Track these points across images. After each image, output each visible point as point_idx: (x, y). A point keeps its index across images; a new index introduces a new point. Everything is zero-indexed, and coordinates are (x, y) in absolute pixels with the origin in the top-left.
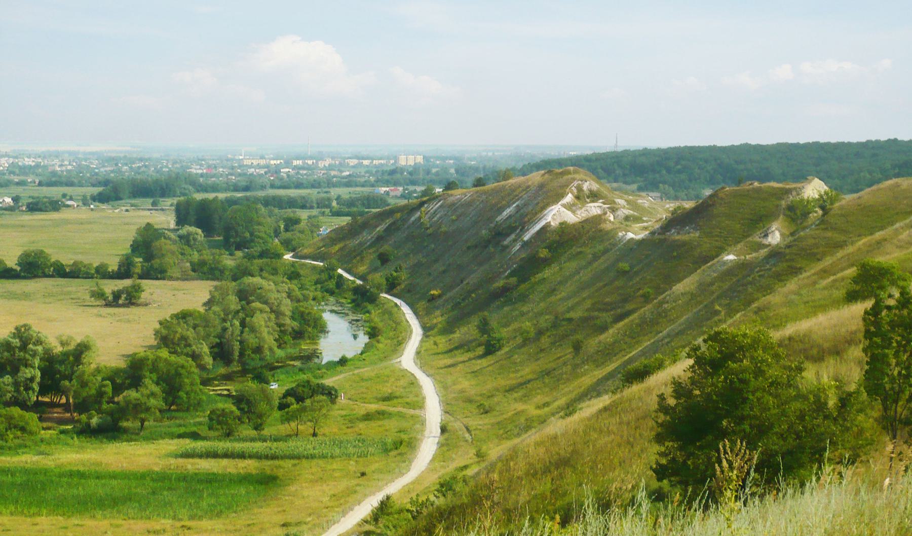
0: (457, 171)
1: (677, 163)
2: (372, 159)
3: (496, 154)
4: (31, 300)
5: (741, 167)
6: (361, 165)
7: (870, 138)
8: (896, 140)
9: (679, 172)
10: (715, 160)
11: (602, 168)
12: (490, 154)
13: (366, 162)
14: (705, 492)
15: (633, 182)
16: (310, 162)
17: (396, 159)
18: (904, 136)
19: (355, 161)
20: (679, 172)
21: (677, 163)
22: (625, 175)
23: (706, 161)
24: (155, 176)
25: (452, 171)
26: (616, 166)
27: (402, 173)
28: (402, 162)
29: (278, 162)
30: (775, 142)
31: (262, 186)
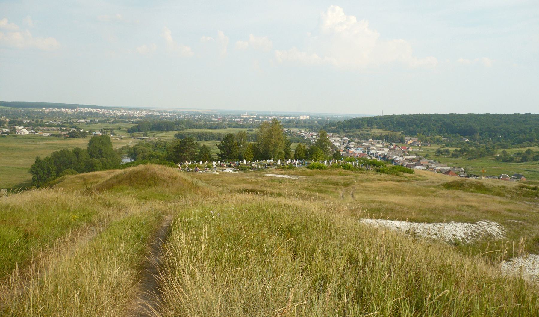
0: (318, 122)
1: (421, 122)
2: (290, 117)
3: (339, 116)
4: (245, 172)
5: (456, 125)
6: (285, 118)
7: (378, 115)
8: (529, 114)
9: (422, 126)
10: (441, 121)
11: (383, 123)
12: (336, 116)
13: (287, 118)
14: (156, 277)
15: (399, 131)
16: (266, 117)
17: (299, 117)
18: (535, 110)
19: (284, 117)
20: (422, 126)
21: (421, 122)
22: (394, 127)
23: (436, 121)
24: (340, 117)
25: (316, 122)
26: (389, 122)
27: (293, 122)
28: (301, 118)
29: (254, 117)
30: (512, 113)
31: (224, 127)
